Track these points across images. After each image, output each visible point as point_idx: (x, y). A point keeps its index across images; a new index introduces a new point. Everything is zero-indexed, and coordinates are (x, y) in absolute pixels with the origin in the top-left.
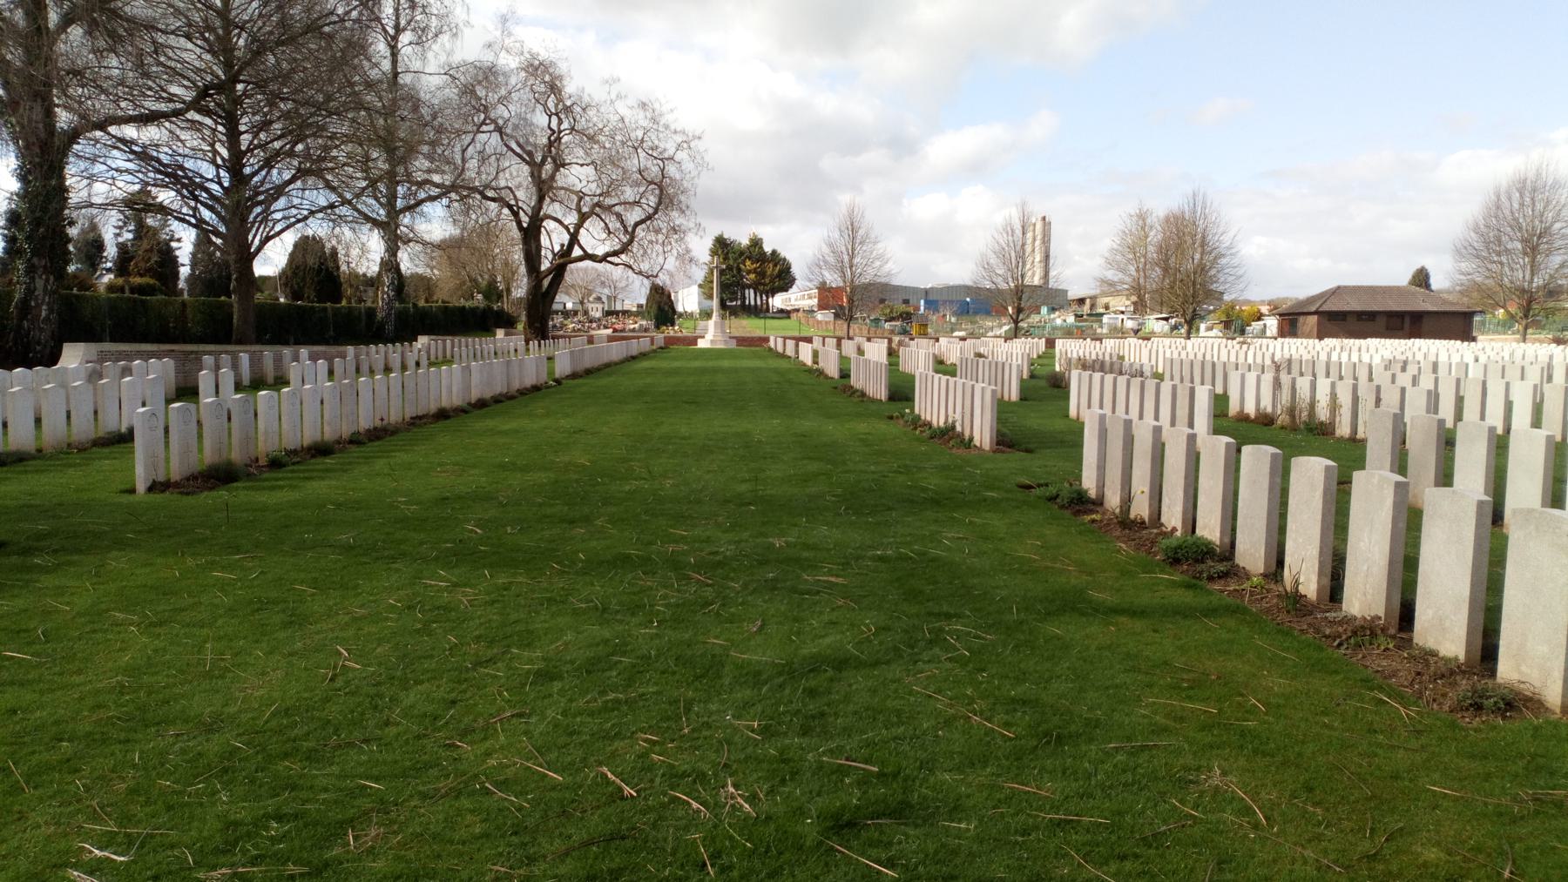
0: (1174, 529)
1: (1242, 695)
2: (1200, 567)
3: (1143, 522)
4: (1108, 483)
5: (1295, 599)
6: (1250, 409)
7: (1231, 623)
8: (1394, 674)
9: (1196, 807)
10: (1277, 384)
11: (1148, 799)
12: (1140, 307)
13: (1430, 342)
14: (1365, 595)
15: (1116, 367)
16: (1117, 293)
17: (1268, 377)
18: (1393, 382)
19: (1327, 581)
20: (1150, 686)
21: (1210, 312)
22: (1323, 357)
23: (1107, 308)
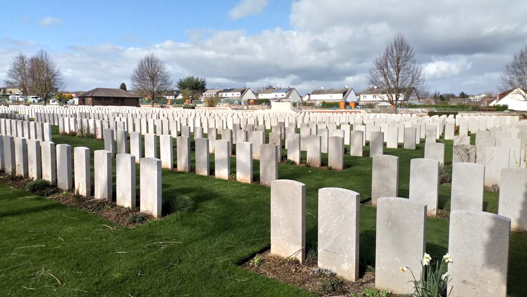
0: (33, 178)
1: (56, 237)
2: (43, 191)
3: (22, 177)
4: (6, 163)
5: (79, 197)
6: (67, 131)
7: (54, 211)
8: (110, 217)
9: (33, 287)
10: (76, 122)
11: (13, 290)
12: (25, 93)
13: (127, 107)
14: (100, 192)
15: (13, 116)
16: (14, 87)
17: (72, 119)
18: (121, 120)
19: (89, 189)
20: (18, 242)
21: (53, 95)
22: (93, 112)
23: (11, 92)
